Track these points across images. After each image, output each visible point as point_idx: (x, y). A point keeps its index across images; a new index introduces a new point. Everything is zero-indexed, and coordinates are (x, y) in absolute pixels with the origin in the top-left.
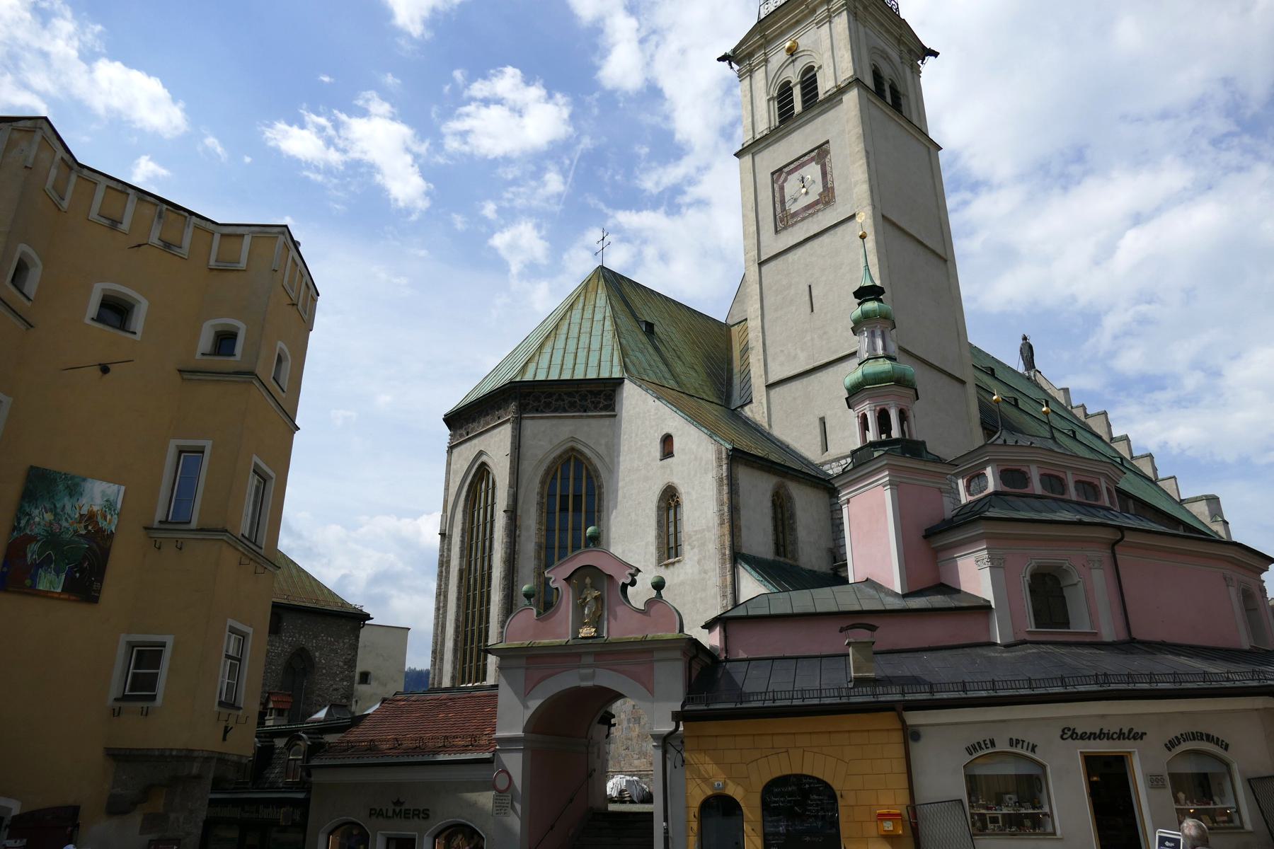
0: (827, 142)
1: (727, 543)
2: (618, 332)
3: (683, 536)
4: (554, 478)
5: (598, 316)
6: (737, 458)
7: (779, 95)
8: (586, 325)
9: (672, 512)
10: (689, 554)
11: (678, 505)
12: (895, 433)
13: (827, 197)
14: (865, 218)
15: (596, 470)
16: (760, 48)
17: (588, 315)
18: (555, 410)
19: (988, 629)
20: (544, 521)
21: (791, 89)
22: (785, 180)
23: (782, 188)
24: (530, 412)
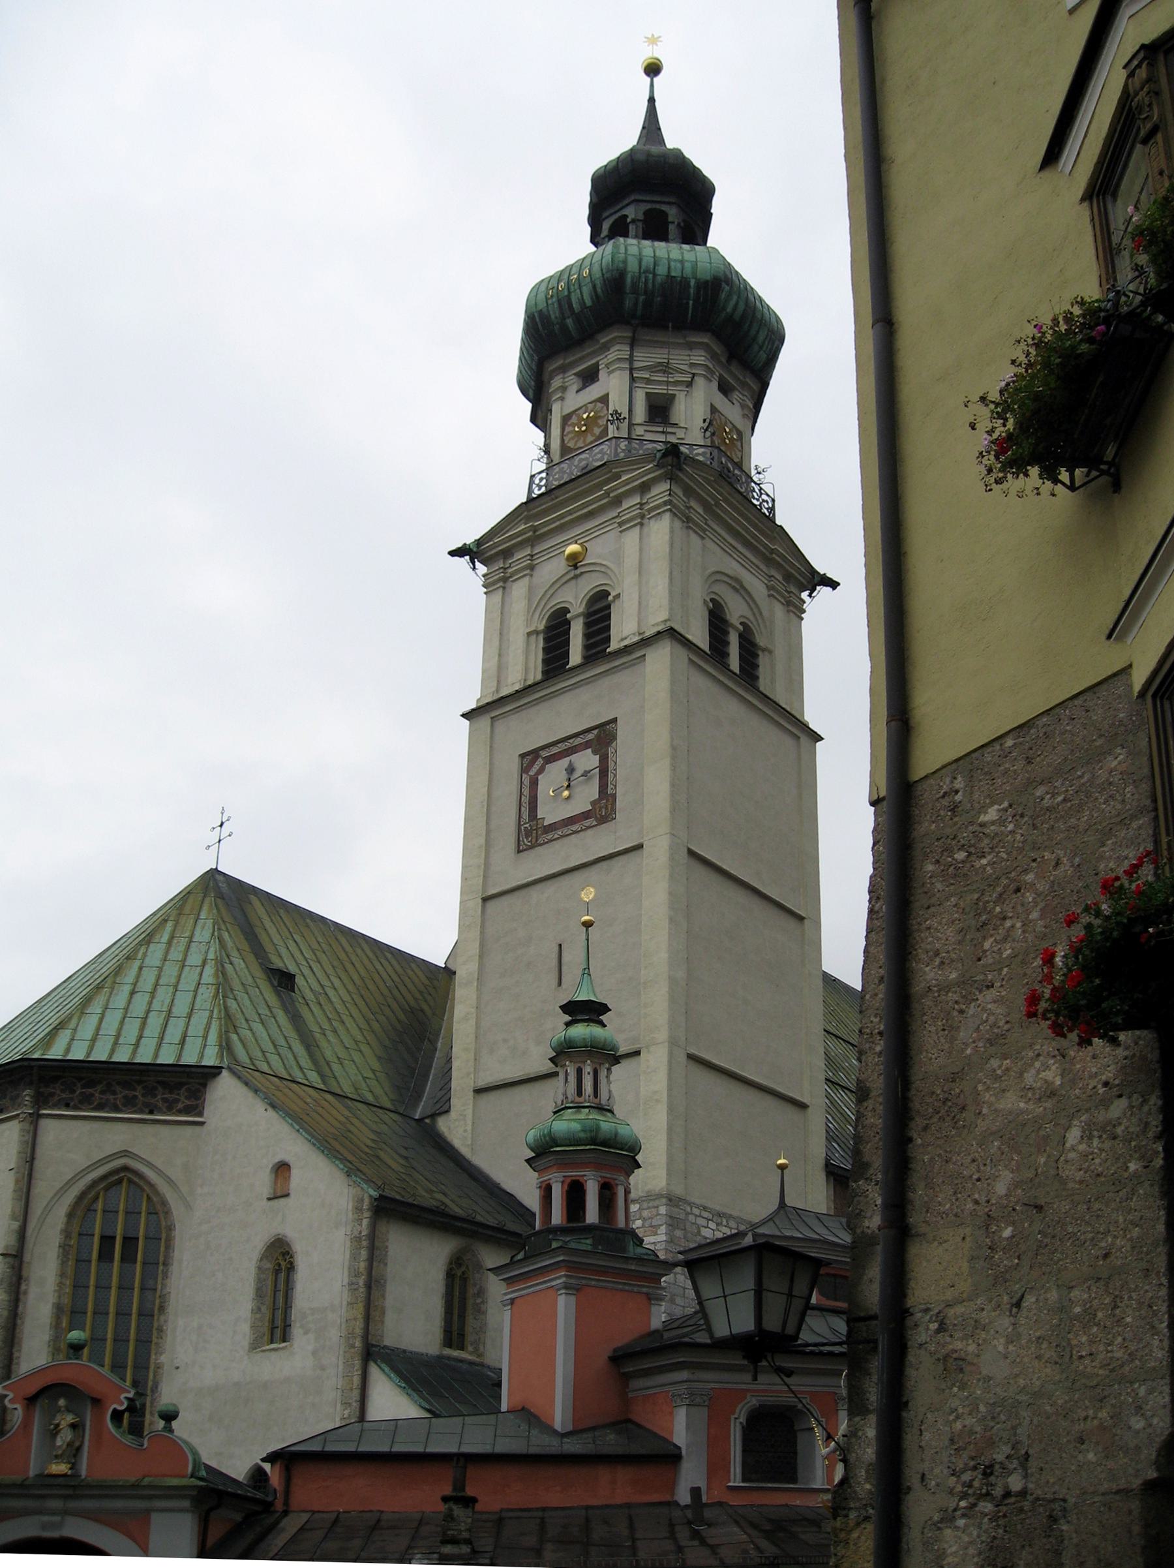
0: (615, 720)
1: (359, 1331)
2: (223, 987)
3: (295, 1314)
4: (90, 1210)
5: (195, 959)
6: (389, 1209)
8: (171, 971)
9: (282, 1275)
11: (291, 1268)
12: (592, 1214)
13: (603, 810)
15: (164, 1203)
16: (521, 545)
17: (176, 954)
19: (672, 1485)
20: (70, 1271)
21: (568, 623)
22: (541, 770)
23: (534, 783)
24: (54, 1107)
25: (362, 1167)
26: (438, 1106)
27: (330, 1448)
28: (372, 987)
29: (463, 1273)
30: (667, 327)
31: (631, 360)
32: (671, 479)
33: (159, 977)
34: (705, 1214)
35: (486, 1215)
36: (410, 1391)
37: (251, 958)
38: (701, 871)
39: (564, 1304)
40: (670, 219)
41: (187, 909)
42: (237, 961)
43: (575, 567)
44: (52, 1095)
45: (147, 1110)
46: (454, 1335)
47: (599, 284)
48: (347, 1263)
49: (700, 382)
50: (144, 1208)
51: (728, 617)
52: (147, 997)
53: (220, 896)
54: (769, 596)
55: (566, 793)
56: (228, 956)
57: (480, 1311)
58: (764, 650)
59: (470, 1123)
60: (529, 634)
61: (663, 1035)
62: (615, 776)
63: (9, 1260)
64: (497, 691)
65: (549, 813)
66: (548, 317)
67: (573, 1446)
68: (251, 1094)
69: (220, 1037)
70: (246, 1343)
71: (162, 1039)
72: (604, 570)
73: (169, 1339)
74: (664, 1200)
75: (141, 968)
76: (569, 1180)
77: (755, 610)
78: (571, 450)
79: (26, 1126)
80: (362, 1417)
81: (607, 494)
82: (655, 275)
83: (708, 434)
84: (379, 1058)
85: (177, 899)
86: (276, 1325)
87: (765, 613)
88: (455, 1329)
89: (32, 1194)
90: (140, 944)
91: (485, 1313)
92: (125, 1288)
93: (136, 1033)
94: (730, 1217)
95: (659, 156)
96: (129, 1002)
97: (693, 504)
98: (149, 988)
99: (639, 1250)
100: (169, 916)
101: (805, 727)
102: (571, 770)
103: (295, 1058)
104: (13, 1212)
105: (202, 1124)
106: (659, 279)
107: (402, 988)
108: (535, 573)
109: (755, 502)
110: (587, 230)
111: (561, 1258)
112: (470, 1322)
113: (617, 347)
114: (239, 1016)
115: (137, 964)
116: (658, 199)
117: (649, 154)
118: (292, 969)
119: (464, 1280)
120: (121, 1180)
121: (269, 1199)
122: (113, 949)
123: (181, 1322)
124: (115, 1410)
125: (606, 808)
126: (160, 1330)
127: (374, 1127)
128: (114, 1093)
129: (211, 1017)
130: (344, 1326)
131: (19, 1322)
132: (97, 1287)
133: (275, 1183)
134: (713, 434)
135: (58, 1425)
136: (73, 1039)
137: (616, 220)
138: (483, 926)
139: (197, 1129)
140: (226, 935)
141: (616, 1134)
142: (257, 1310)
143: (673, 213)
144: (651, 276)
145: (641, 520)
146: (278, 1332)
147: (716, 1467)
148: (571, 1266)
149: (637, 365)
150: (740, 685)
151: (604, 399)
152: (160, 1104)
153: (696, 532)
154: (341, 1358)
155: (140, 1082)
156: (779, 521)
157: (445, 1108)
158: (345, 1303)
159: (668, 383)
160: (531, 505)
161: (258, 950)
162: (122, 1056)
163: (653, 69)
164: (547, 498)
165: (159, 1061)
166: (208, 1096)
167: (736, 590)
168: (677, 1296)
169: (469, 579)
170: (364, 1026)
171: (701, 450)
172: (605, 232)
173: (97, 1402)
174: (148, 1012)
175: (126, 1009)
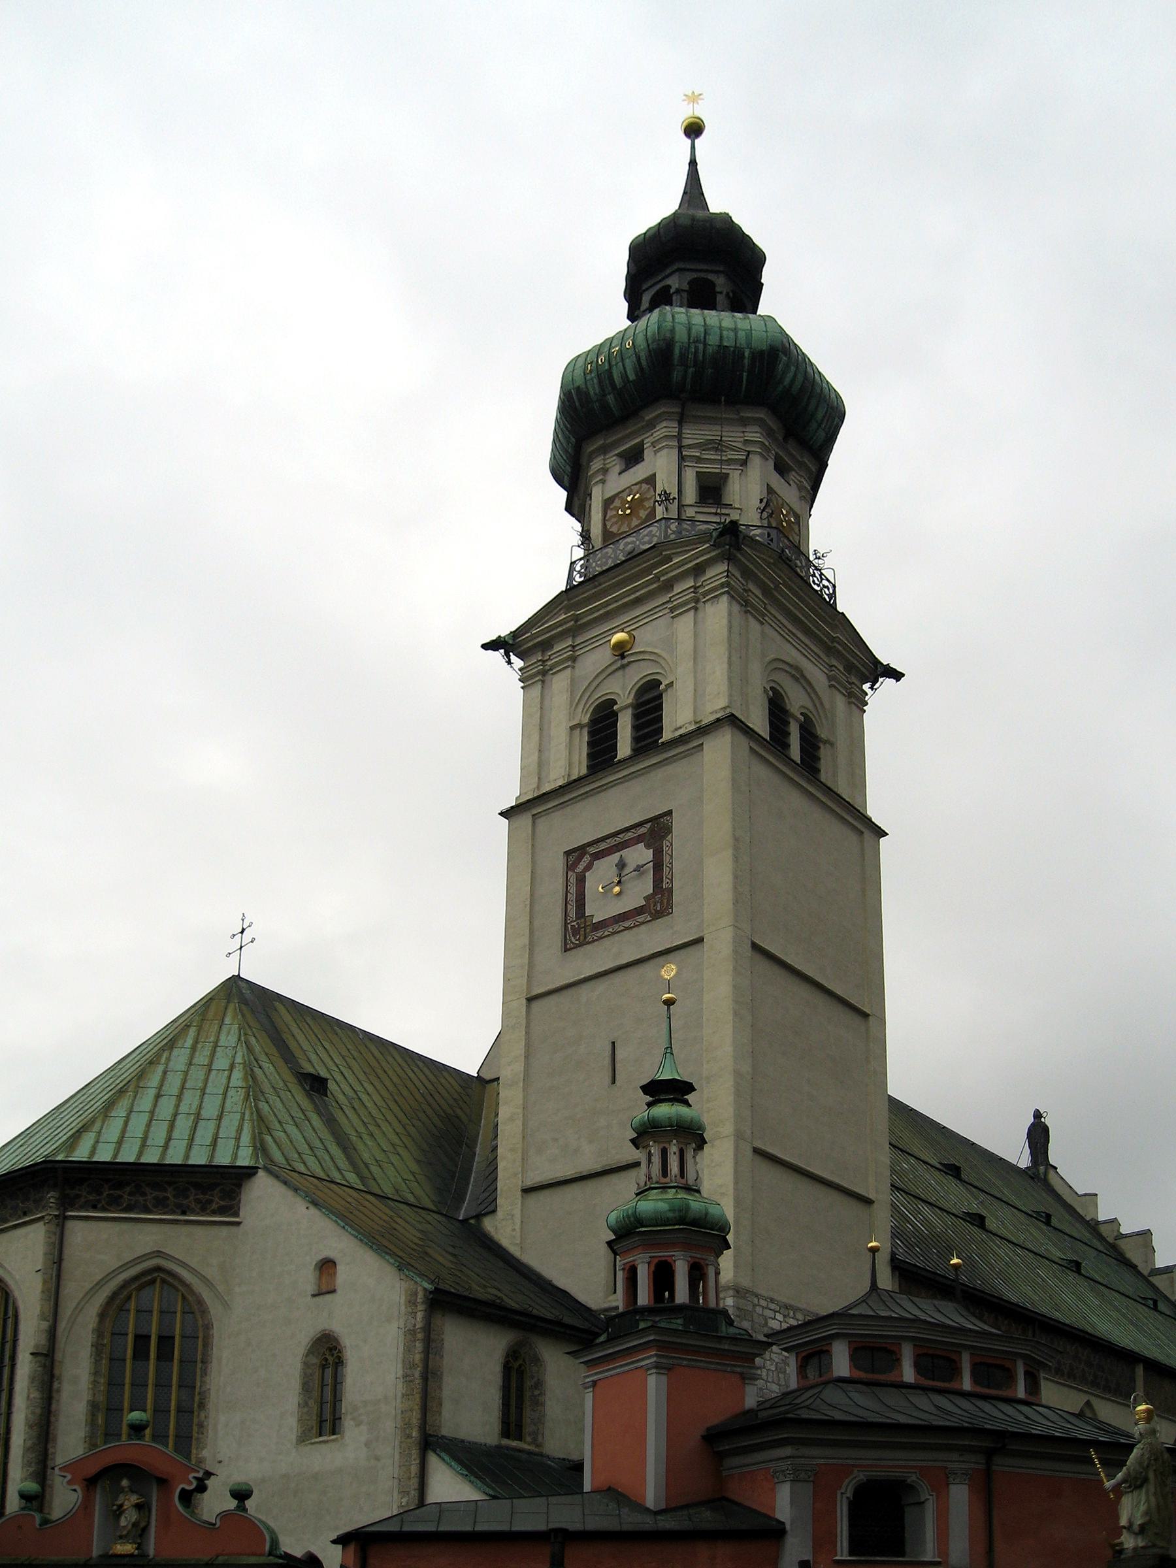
0: (670, 813)
2: (253, 1090)
3: (345, 1406)
4: (123, 1309)
5: (222, 1062)
6: (443, 1302)
7: (593, 722)
8: (197, 1075)
9: (329, 1372)
10: (353, 1434)
11: (339, 1362)
12: (682, 1294)
13: (659, 904)
14: (721, 944)
15: (200, 1302)
16: (562, 636)
17: (201, 1058)
18: (128, 1209)
20: (104, 1369)
22: (589, 867)
23: (581, 880)
24: (80, 1208)
25: (412, 1262)
26: (482, 1207)
27: (407, 1528)
28: (405, 1092)
29: (520, 1366)
30: (719, 402)
31: (679, 437)
32: (729, 559)
33: (184, 1081)
34: (772, 1306)
35: (544, 1310)
36: (472, 1478)
37: (281, 1063)
38: (764, 965)
39: (654, 1384)
40: (718, 289)
41: (210, 1015)
42: (266, 1065)
43: (622, 656)
44: (78, 1196)
45: (179, 1211)
46: (511, 1424)
47: (643, 355)
48: (401, 1356)
49: (756, 461)
50: (179, 1308)
51: (788, 707)
52: (173, 1100)
53: (244, 1001)
54: (830, 686)
55: (617, 889)
56: (256, 1060)
57: (538, 1403)
58: (826, 742)
59: (518, 1222)
60: (572, 728)
61: (728, 1129)
62: (671, 869)
63: (39, 1358)
64: (538, 788)
65: (598, 911)
66: (587, 394)
67: (667, 1523)
68: (290, 1193)
69: (254, 1138)
70: (293, 1437)
71: (192, 1140)
72: (655, 658)
73: (211, 1433)
74: (731, 1292)
75: (165, 1073)
76: (656, 1260)
77: (817, 701)
78: (613, 535)
79: (53, 1228)
80: (421, 1503)
81: (657, 578)
82: (705, 344)
83: (765, 515)
84: (418, 1162)
85: (192, 1011)
86: (324, 1415)
87: (827, 705)
88: (514, 1418)
89: (61, 1295)
90: (162, 1049)
91: (543, 1404)
92: (162, 1385)
93: (164, 1135)
94: (796, 1309)
95: (705, 221)
96: (155, 1105)
97: (751, 586)
98: (175, 1091)
99: (732, 1330)
100: (191, 1021)
101: (868, 821)
102: (621, 865)
103: (332, 1159)
104: (42, 1313)
105: (238, 1224)
106: (710, 350)
107: (437, 1096)
108: (577, 665)
109: (815, 587)
110: (625, 305)
111: (652, 1338)
112: (528, 1414)
113: (664, 424)
114: (273, 1118)
115: (161, 1068)
116: (705, 267)
117: (693, 219)
118: (323, 1073)
119: (521, 1373)
120: (156, 1277)
121: (314, 1296)
122: (134, 1055)
123: (222, 1418)
124: (183, 1489)
125: (662, 903)
126: (201, 1425)
127: (420, 1227)
128: (144, 1194)
129: (242, 1119)
130: (399, 1417)
131: (53, 1419)
132: (132, 1385)
133: (320, 1278)
134: (771, 515)
135: (121, 1506)
136: (97, 1142)
137: (657, 294)
138: (528, 1026)
139: (233, 1229)
140: (253, 1040)
141: (707, 1214)
142: (303, 1405)
143: (720, 282)
144: (701, 346)
145: (696, 603)
146: (327, 1426)
147: (823, 1540)
148: (661, 1346)
149: (686, 442)
150: (803, 776)
151: (651, 480)
152: (193, 1205)
153: (755, 617)
154: (397, 1447)
155: (170, 1184)
156: (840, 609)
157: (490, 1209)
158: (399, 1395)
159: (721, 462)
160: (571, 594)
161: (287, 1055)
162: (151, 1157)
163: (694, 130)
164: (588, 586)
165: (190, 1162)
166: (244, 1197)
167: (797, 680)
168: (776, 1374)
169: (505, 675)
170: (400, 1130)
171: (758, 531)
172: (645, 304)
173: (163, 1482)
174: (175, 1115)
175: (152, 1113)
